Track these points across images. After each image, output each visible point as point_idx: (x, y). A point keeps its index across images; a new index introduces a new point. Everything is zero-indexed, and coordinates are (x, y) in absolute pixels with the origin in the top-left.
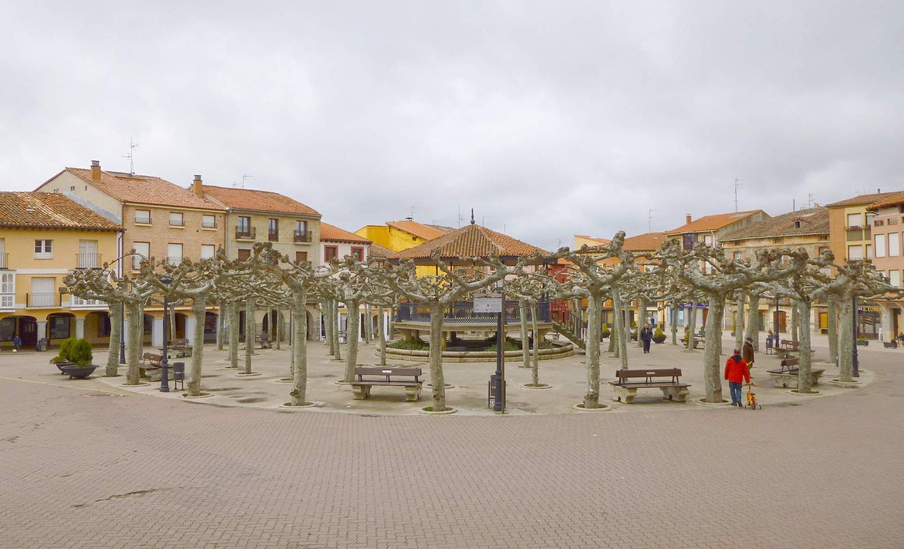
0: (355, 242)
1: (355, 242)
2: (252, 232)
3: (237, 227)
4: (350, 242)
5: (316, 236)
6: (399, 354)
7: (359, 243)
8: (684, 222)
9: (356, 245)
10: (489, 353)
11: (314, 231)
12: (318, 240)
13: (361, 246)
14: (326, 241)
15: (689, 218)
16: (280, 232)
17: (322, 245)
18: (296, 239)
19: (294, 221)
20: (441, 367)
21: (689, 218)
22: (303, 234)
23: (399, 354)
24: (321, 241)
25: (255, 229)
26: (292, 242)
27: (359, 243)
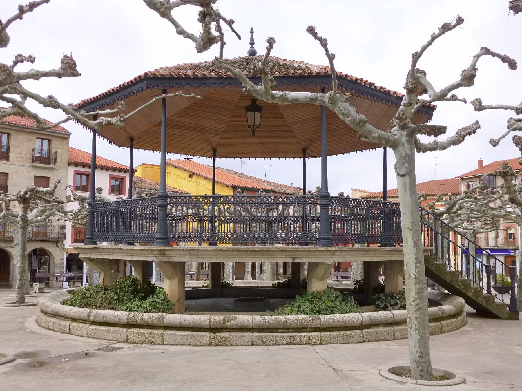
0: (114, 169)
1: (114, 169)
2: (53, 157)
3: (33, 150)
4: (107, 169)
5: (62, 158)
6: (65, 317)
7: (120, 170)
8: (476, 167)
9: (116, 174)
10: (292, 319)
11: (59, 152)
12: (65, 164)
13: (122, 174)
14: (77, 164)
15: (480, 162)
16: (12, 149)
17: (71, 170)
18: (34, 160)
19: (34, 137)
20: (427, 343)
21: (480, 162)
22: (45, 154)
23: (65, 317)
24: (70, 164)
25: (56, 153)
26: (28, 163)
27: (120, 170)
